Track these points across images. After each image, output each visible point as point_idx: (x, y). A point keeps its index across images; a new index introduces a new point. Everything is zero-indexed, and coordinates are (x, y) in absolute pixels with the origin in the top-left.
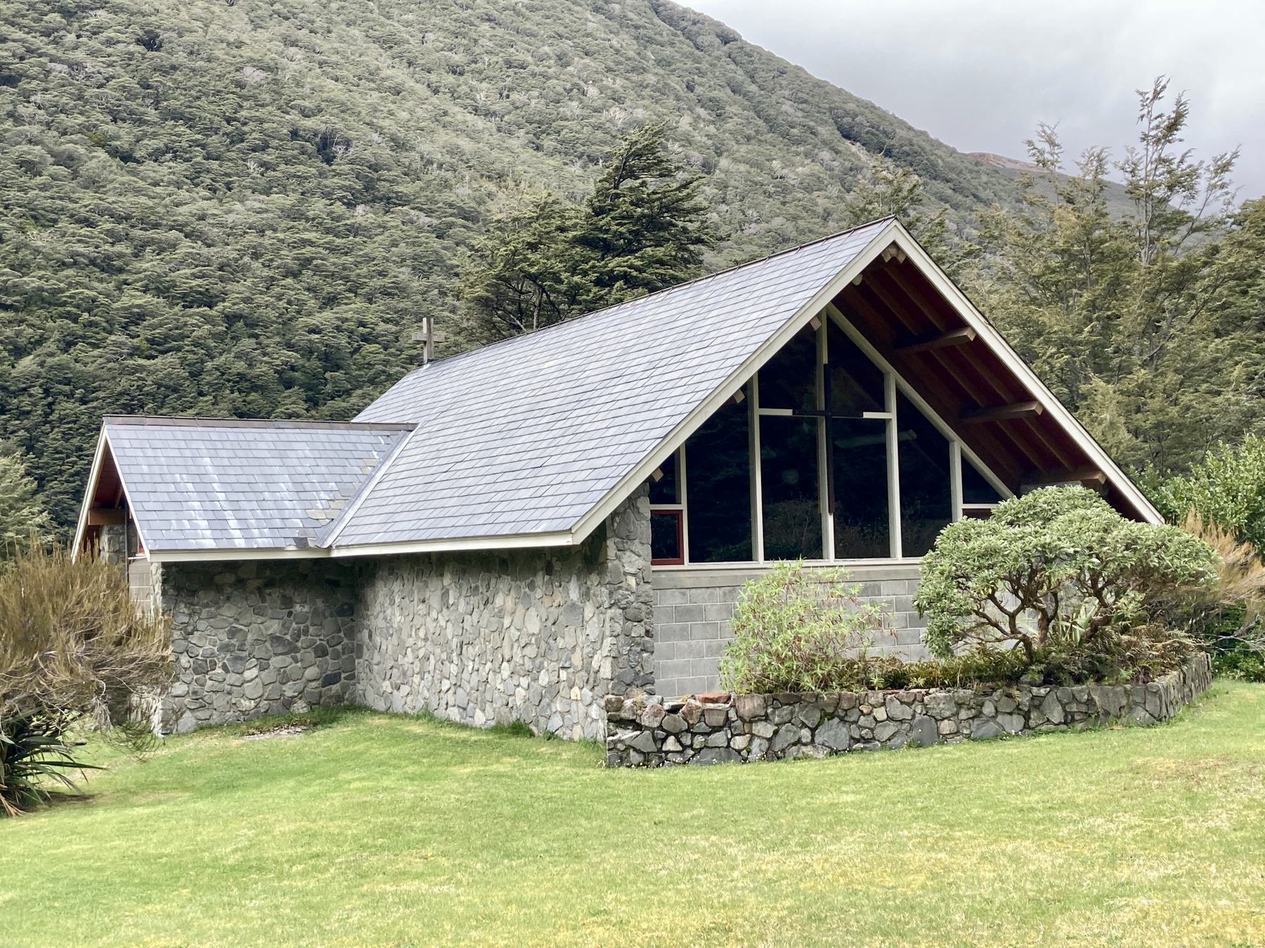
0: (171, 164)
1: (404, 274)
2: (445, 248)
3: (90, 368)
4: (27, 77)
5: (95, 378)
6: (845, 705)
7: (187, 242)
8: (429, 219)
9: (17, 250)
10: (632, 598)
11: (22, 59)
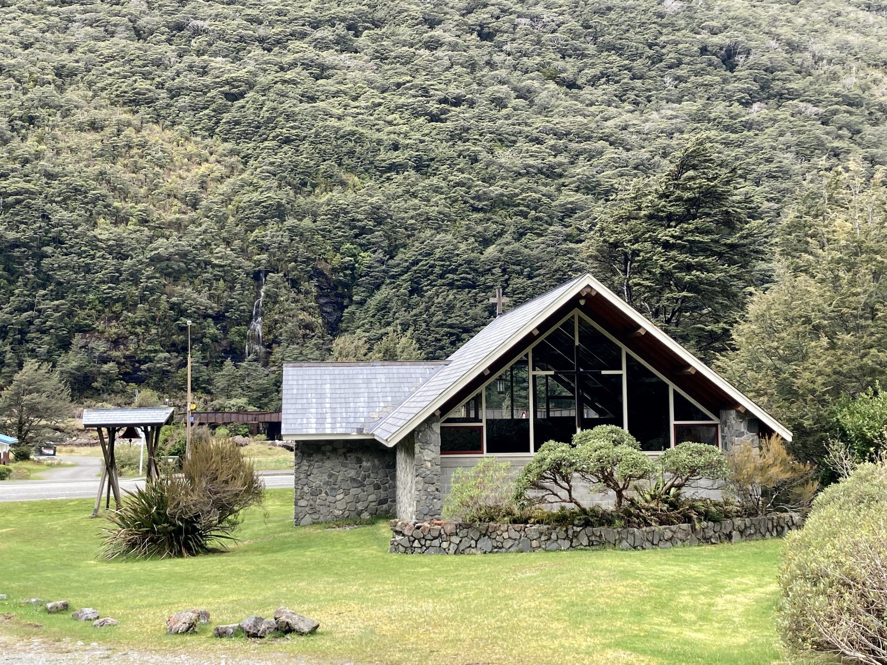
0: (605, 86)
1: (787, 159)
2: (828, 133)
3: (535, 252)
4: (501, 32)
5: (539, 259)
6: (490, 530)
7: (611, 149)
8: (816, 109)
9: (487, 166)
10: (428, 472)
11: (498, 18)
